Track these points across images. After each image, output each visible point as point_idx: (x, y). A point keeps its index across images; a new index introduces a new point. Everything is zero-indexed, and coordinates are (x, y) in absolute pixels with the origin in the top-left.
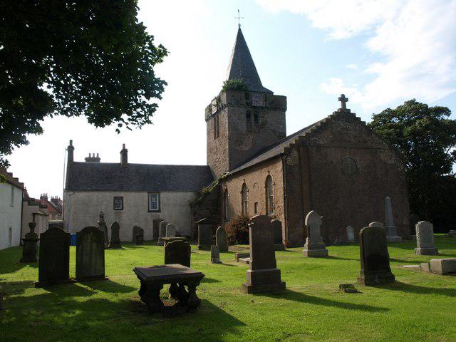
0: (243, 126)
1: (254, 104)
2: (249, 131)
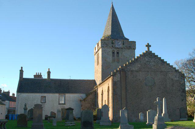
0: (110, 58)
1: (117, 46)
2: (114, 61)
